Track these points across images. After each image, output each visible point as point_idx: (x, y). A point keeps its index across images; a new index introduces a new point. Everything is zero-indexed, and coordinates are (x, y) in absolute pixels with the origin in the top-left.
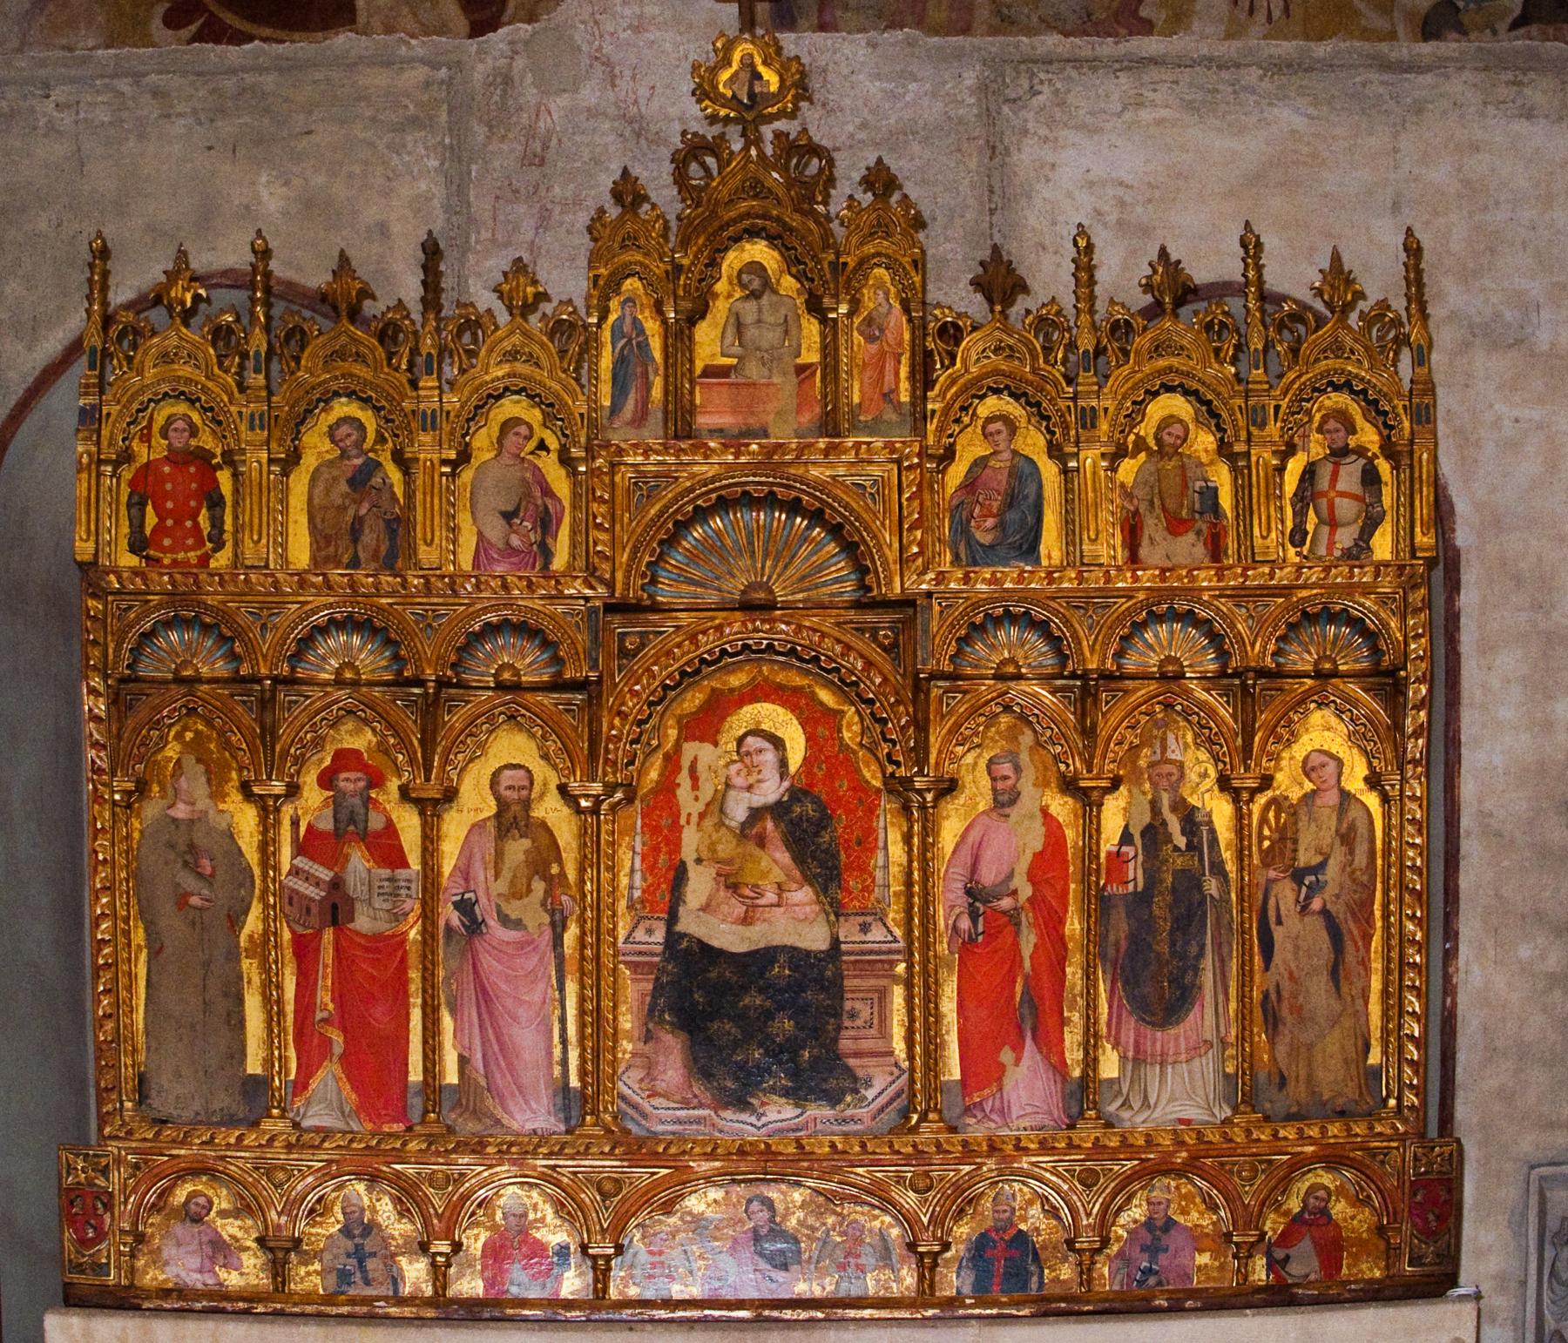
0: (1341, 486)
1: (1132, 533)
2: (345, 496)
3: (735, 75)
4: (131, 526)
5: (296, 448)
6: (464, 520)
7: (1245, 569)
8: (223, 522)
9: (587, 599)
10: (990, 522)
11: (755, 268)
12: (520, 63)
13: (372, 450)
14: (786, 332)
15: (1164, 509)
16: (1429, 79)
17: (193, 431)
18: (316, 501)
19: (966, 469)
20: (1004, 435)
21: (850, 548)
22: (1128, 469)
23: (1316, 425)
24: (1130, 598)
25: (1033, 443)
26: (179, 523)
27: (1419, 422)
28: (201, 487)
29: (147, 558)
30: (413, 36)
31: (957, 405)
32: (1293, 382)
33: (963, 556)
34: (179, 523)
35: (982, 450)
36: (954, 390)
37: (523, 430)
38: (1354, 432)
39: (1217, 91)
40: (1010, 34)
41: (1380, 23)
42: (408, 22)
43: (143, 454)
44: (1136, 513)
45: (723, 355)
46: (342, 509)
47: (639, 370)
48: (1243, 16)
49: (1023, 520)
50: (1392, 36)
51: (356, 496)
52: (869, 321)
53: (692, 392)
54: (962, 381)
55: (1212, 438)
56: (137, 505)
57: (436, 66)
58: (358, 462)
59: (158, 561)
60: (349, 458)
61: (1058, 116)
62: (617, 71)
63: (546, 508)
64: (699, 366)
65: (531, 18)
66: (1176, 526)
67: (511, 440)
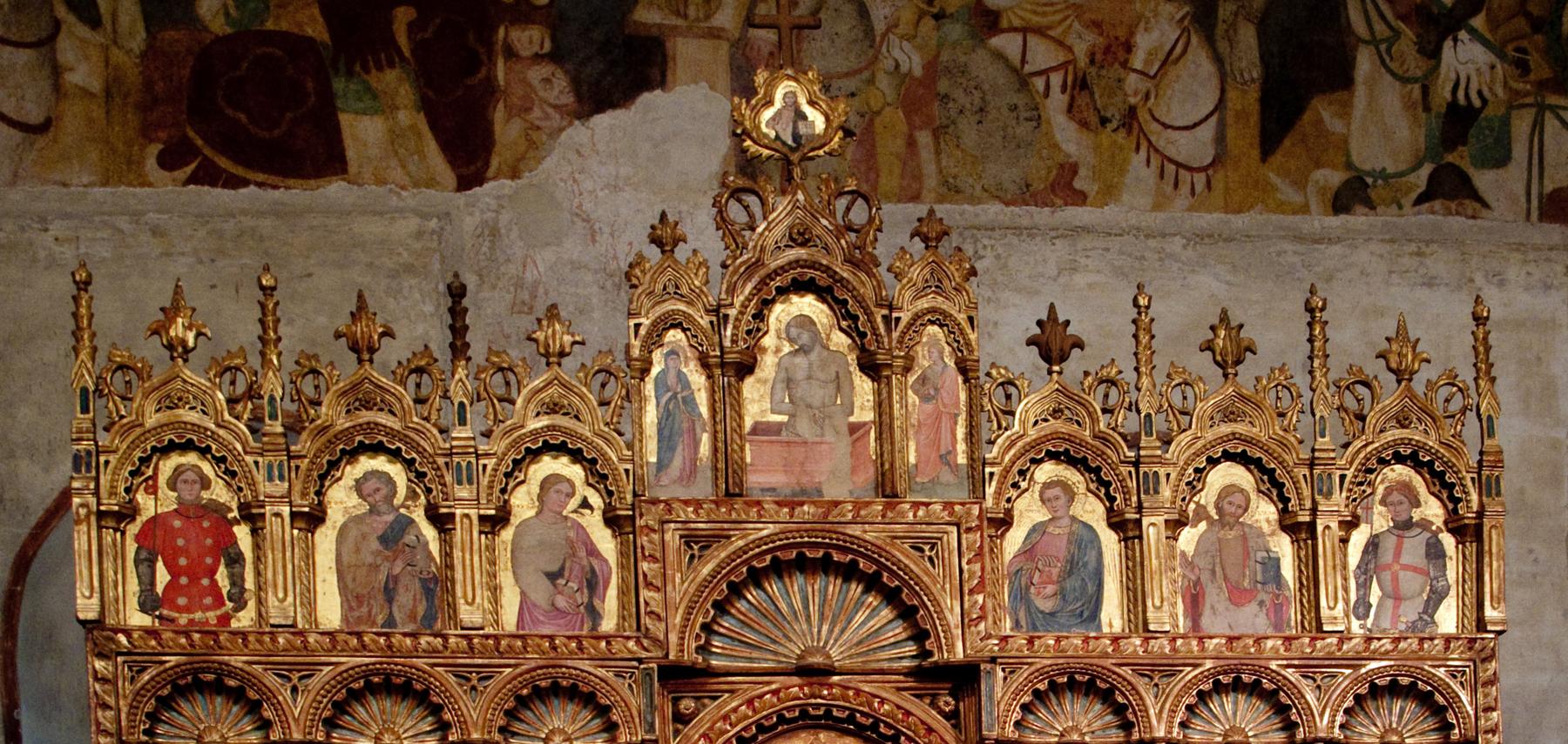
0: (1405, 559)
1: (1195, 603)
2: (377, 553)
3: (778, 114)
4: (140, 583)
5: (320, 503)
6: (506, 579)
7: (1313, 639)
8: (243, 580)
9: (640, 661)
10: (1050, 589)
11: (804, 321)
12: (505, 218)
13: (403, 506)
14: (838, 389)
15: (1226, 578)
16: (1337, 249)
17: (205, 484)
18: (345, 559)
19: (1024, 535)
20: (1063, 500)
21: (907, 613)
22: (1188, 538)
23: (1378, 497)
24: (1196, 666)
25: (1091, 511)
26: (194, 579)
27: (1489, 495)
28: (217, 543)
29: (160, 617)
30: (403, 188)
31: (1015, 469)
32: (1359, 451)
33: (1023, 623)
34: (194, 579)
35: (1041, 515)
36: (1012, 452)
37: (565, 487)
38: (1418, 504)
39: (1143, 257)
40: (957, 203)
41: (1298, 199)
42: (397, 174)
43: (148, 506)
44: (1198, 582)
45: (773, 412)
46: (374, 568)
47: (685, 425)
48: (1169, 189)
49: (1084, 588)
50: (1305, 209)
51: (387, 553)
52: (923, 379)
53: (742, 449)
54: (1020, 444)
55: (1273, 509)
56: (146, 563)
57: (425, 216)
58: (390, 518)
59: (173, 620)
60: (379, 514)
61: (1000, 278)
62: (596, 227)
63: (593, 571)
64: (748, 423)
65: (515, 174)
66: (1238, 596)
67: (552, 495)
